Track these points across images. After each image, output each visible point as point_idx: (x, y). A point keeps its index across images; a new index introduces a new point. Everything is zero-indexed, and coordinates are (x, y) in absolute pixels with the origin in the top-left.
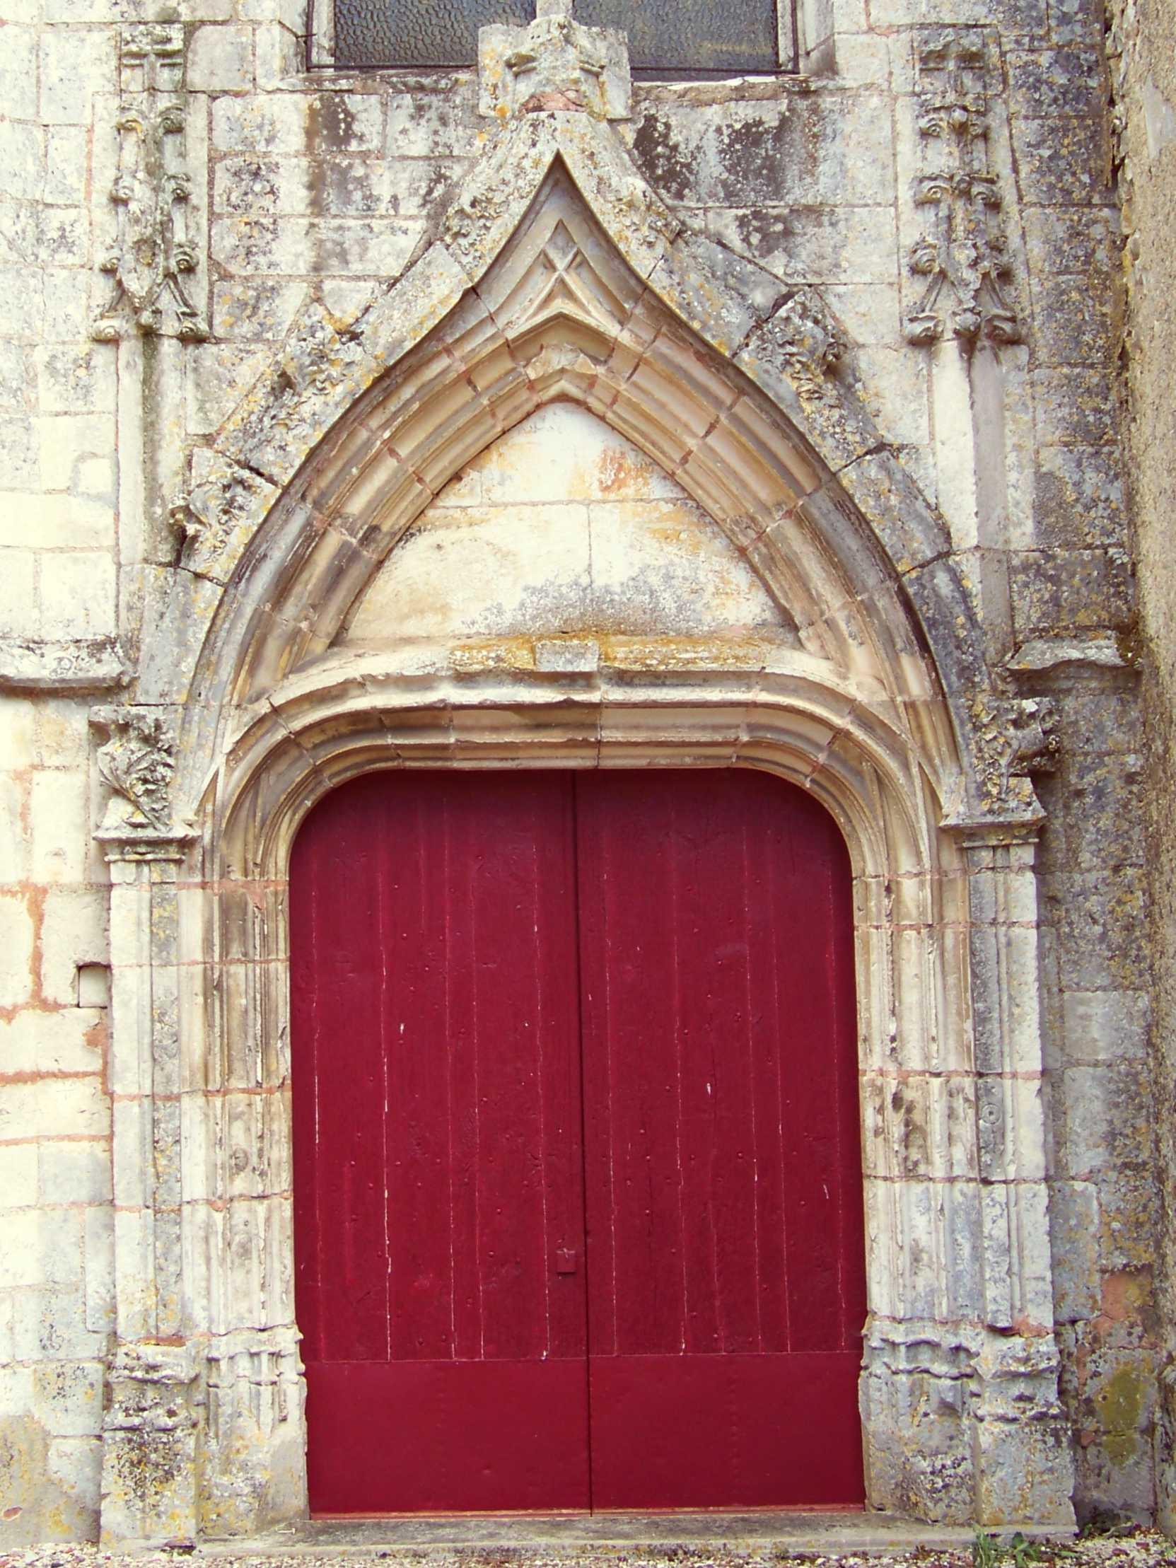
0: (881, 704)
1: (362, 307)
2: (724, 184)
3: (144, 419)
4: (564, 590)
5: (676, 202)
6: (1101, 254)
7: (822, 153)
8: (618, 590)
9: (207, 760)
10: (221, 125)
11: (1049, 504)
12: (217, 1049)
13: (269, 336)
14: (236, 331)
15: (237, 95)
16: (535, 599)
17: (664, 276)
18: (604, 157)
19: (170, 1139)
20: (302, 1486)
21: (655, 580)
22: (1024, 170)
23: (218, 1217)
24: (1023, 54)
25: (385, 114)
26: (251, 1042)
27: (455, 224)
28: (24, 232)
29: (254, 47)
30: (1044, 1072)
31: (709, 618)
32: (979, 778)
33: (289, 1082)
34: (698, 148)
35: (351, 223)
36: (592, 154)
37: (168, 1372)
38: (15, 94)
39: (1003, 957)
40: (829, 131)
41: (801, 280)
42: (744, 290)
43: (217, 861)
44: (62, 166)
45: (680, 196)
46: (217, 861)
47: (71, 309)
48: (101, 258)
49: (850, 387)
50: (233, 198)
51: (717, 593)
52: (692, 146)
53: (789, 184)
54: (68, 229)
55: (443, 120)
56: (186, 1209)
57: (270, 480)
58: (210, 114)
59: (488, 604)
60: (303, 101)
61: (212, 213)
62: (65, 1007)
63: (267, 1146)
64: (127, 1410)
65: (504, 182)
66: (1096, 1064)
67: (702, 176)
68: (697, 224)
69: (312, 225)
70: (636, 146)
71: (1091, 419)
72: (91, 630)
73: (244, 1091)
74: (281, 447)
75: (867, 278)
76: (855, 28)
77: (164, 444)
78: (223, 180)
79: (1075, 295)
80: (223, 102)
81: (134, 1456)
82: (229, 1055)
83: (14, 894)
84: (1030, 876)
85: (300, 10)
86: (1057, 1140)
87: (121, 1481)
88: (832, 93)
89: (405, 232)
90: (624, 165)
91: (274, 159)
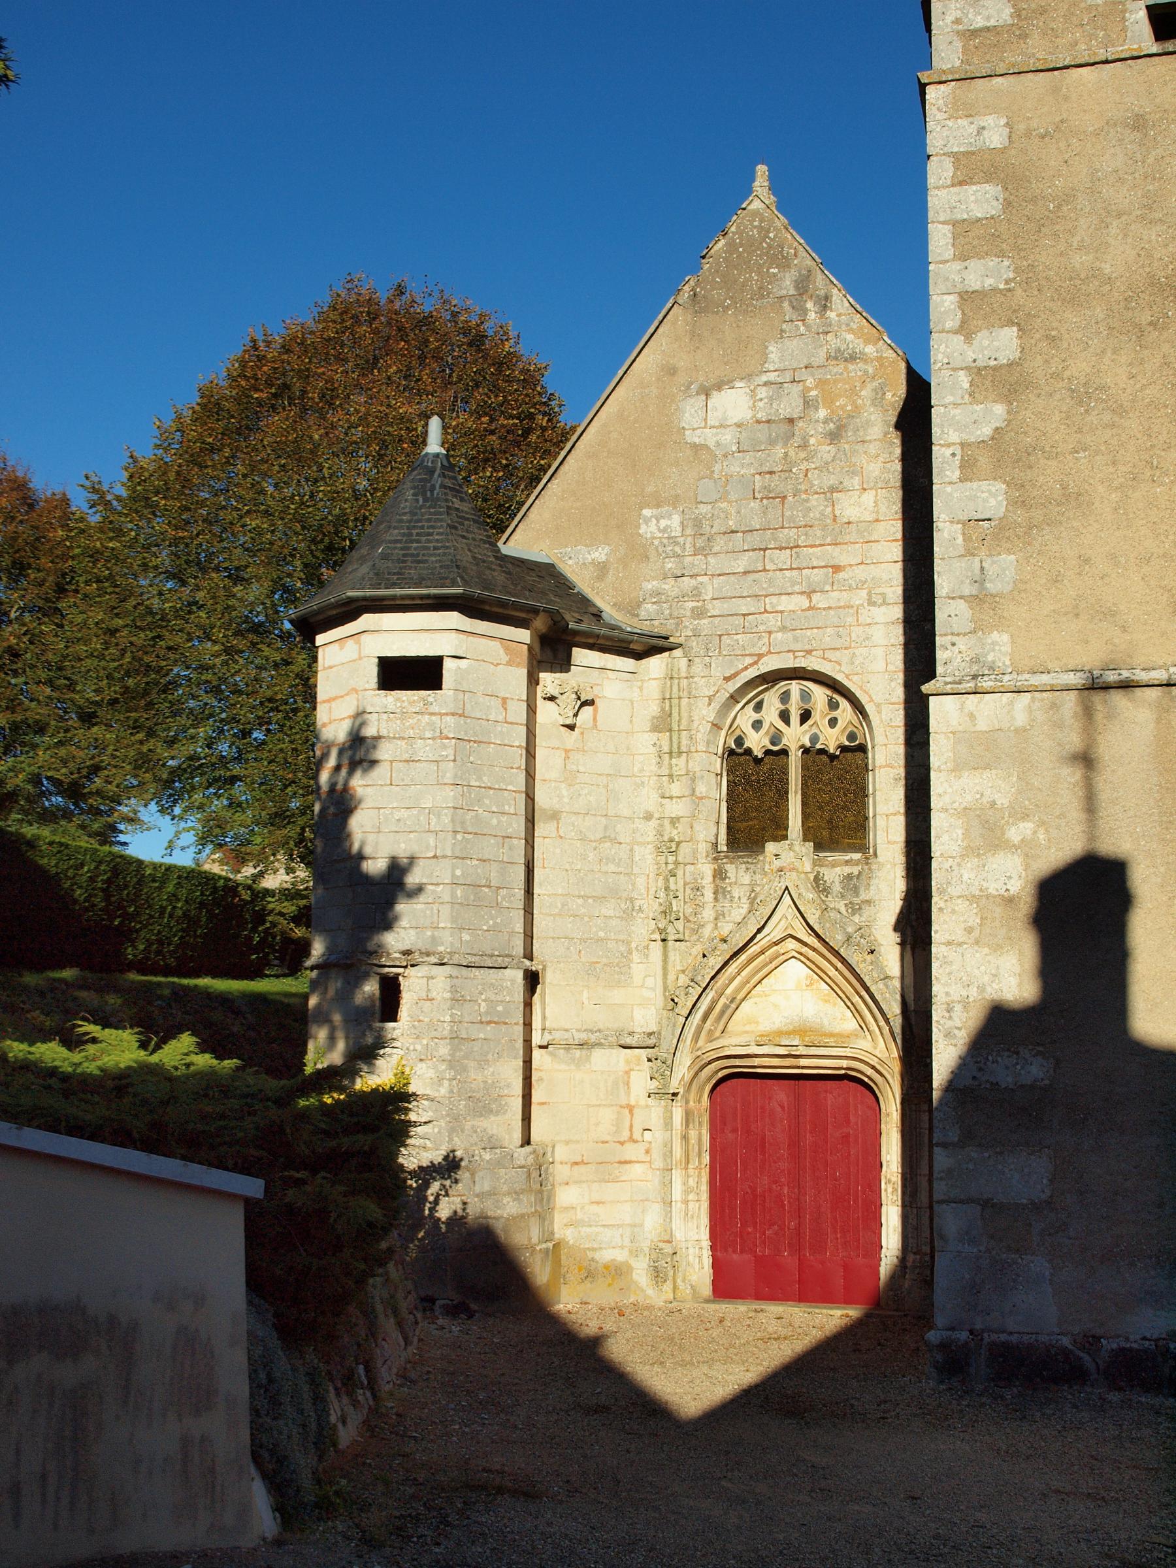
10: (687, 874)
18: (801, 886)
48: (651, 915)
60: (712, 866)
68: (832, 906)
78: (688, 891)
80: (688, 867)
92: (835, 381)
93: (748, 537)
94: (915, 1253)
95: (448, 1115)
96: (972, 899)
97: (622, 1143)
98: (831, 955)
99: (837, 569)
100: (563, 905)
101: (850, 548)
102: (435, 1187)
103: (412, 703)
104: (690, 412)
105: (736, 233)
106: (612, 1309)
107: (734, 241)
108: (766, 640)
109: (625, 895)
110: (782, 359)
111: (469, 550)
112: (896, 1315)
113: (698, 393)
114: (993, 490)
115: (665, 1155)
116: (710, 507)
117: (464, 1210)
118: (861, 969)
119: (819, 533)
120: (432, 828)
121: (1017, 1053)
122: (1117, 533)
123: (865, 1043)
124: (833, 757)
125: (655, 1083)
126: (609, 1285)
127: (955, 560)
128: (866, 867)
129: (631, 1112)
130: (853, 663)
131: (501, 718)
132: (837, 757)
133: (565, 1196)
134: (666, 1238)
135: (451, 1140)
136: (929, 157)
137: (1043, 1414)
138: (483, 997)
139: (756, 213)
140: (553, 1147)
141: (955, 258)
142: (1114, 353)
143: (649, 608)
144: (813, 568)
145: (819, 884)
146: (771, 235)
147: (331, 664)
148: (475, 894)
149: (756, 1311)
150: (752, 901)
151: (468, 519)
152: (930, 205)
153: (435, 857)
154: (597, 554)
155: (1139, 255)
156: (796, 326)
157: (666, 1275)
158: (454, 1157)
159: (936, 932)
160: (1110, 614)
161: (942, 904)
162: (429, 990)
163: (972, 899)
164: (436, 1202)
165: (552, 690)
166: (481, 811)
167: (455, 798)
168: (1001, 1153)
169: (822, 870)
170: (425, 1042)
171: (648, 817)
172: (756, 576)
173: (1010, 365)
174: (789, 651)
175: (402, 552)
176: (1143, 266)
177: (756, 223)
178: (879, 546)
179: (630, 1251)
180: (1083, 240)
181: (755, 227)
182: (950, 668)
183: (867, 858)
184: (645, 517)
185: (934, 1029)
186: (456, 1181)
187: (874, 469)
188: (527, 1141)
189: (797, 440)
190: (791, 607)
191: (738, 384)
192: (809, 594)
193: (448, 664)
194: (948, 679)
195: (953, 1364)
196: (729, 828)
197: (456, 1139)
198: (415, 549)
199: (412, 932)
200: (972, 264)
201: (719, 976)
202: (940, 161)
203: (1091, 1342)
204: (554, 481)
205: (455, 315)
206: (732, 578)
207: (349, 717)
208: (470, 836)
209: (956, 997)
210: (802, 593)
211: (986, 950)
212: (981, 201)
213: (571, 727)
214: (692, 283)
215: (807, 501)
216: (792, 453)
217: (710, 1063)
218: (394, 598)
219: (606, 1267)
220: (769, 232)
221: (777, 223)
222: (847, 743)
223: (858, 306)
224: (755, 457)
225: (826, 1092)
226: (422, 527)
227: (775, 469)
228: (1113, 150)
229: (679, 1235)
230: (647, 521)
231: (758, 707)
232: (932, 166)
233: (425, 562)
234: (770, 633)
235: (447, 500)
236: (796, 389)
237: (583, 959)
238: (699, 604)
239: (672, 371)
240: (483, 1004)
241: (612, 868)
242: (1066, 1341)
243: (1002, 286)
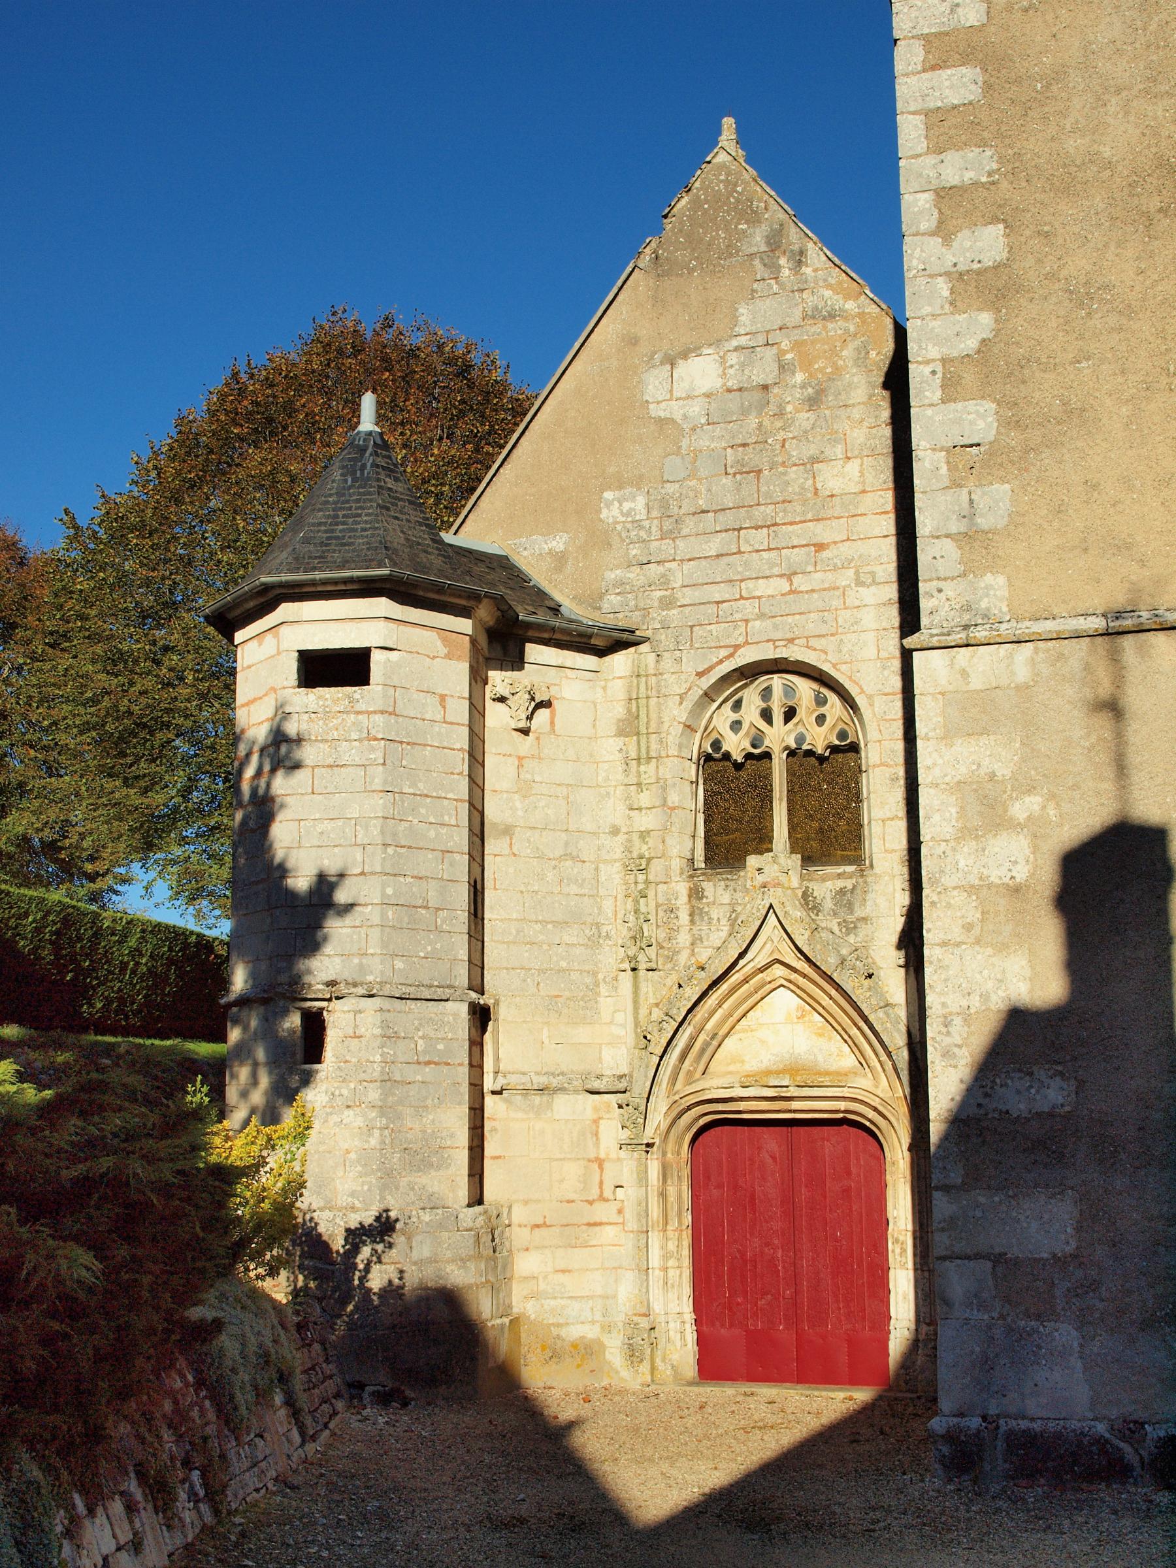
10: (660, 894)
18: (787, 904)
48: (620, 942)
55: (735, 890)
60: (687, 885)
68: (823, 925)
78: (661, 914)
80: (660, 886)
92: (812, 343)
93: (720, 516)
95: (379, 1170)
96: (971, 890)
97: (591, 1203)
98: (826, 984)
99: (820, 547)
100: (518, 932)
101: (834, 523)
102: (366, 1252)
103: (336, 701)
104: (654, 384)
105: (701, 189)
107: (698, 197)
108: (743, 629)
109: (589, 920)
110: (753, 322)
111: (402, 532)
112: (909, 1393)
113: (662, 363)
114: (982, 410)
115: (639, 1214)
116: (677, 485)
117: (401, 1279)
118: (858, 996)
119: (799, 509)
120: (359, 841)
121: (1031, 1074)
122: (1130, 452)
123: (865, 1082)
124: (822, 759)
126: (578, 1366)
127: (939, 493)
128: (861, 880)
129: (601, 1167)
130: (840, 651)
131: (439, 717)
132: (827, 758)
133: (525, 1264)
134: (644, 1310)
135: (383, 1198)
136: (896, 41)
137: (1073, 1523)
138: (420, 1033)
139: (723, 166)
140: (510, 1207)
141: (929, 151)
142: (1118, 246)
143: (612, 601)
144: (793, 547)
145: (808, 901)
146: (739, 189)
147: (250, 663)
148: (410, 913)
149: (745, 1394)
150: (733, 922)
151: (401, 500)
152: (898, 94)
153: (362, 873)
154: (554, 543)
155: (1143, 134)
156: (769, 285)
158: (388, 1217)
159: (929, 931)
160: (1125, 547)
161: (935, 898)
162: (356, 1026)
163: (971, 890)
164: (367, 1269)
165: (503, 690)
166: (416, 821)
167: (385, 806)
168: (1014, 1196)
169: (811, 885)
170: (352, 1086)
171: (615, 831)
172: (731, 558)
173: (997, 267)
174: (768, 641)
175: (325, 535)
176: (1149, 146)
177: (722, 178)
178: (866, 519)
179: (602, 1328)
180: (1077, 122)
181: (722, 181)
182: (936, 619)
183: (862, 870)
184: (606, 500)
185: (930, 1048)
186: (390, 1246)
187: (858, 435)
188: (477, 1199)
189: (772, 409)
190: (770, 592)
191: (706, 351)
192: (789, 577)
193: (376, 657)
194: (934, 631)
195: (963, 1457)
196: (707, 842)
197: (389, 1197)
198: (341, 531)
199: (337, 960)
200: (949, 156)
201: (697, 1009)
202: (909, 45)
203: (1132, 1429)
204: (507, 466)
205: (440, 347)
206: (703, 562)
207: (268, 720)
208: (403, 850)
209: (954, 1008)
210: (781, 576)
211: (989, 951)
212: (958, 85)
213: (525, 732)
214: (653, 245)
215: (785, 474)
216: (766, 423)
217: (689, 1108)
218: (313, 583)
219: (575, 1346)
220: (736, 185)
221: (746, 176)
222: (837, 742)
223: (836, 260)
224: (726, 429)
225: (823, 1139)
226: (350, 509)
227: (749, 441)
228: (1108, 19)
229: (657, 1307)
230: (609, 505)
231: (737, 706)
232: (900, 52)
233: (353, 544)
234: (747, 621)
235: (378, 480)
236: (770, 353)
237: (542, 993)
238: (668, 593)
239: (634, 341)
240: (420, 1042)
241: (574, 889)
242: (1101, 1428)
243: (984, 179)
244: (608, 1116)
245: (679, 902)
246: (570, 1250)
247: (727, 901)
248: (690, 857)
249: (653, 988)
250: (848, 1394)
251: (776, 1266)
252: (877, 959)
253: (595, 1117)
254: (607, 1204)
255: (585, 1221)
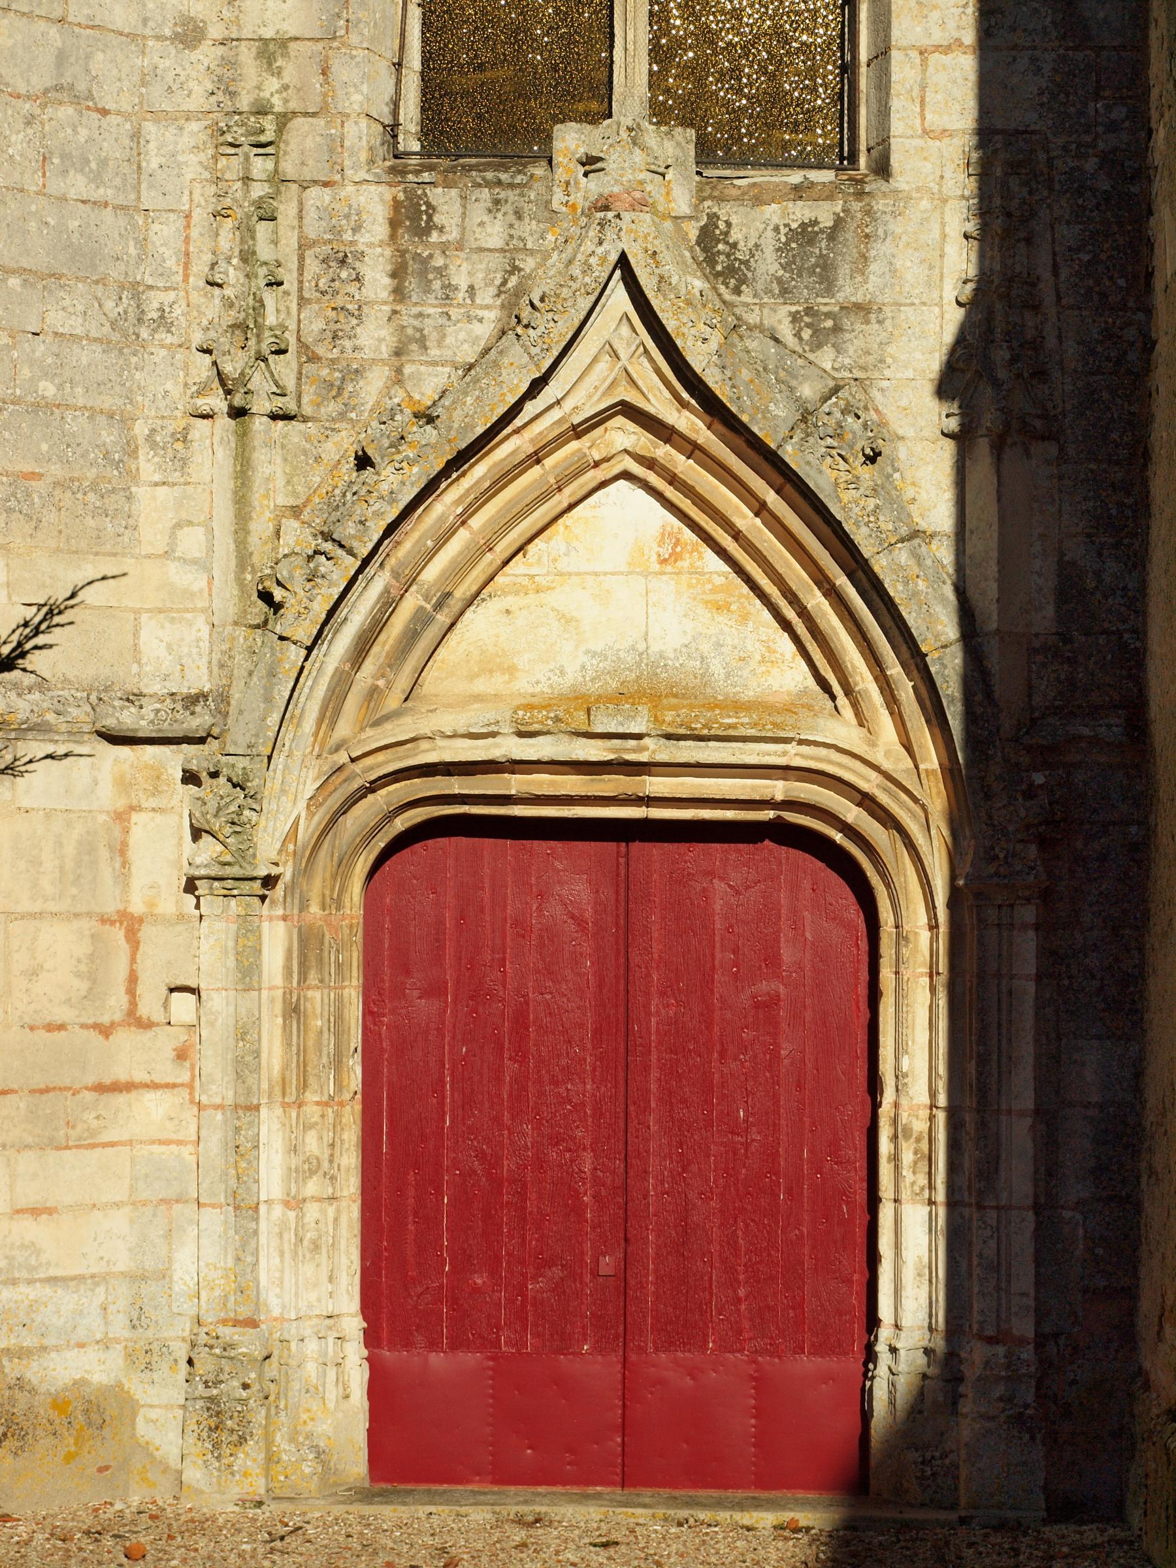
0: (907, 771)
1: (439, 390)
2: (780, 281)
3: (236, 493)
4: (622, 654)
5: (734, 298)
6: (1132, 356)
7: (873, 253)
8: (672, 656)
9: (290, 805)
10: (311, 215)
11: (1069, 588)
12: (294, 1065)
13: (353, 415)
14: (323, 410)
15: (326, 184)
16: (594, 662)
17: (716, 371)
18: (665, 256)
19: (249, 1145)
20: (364, 1455)
21: (705, 647)
22: (1064, 273)
23: (292, 1215)
24: (1069, 160)
25: (464, 207)
26: (325, 1060)
27: (526, 313)
28: (126, 312)
29: (342, 141)
30: (1037, 1111)
31: (755, 684)
32: (987, 843)
33: (359, 1096)
34: (757, 246)
35: (431, 311)
36: (655, 253)
37: (244, 1350)
38: (118, 181)
39: (1004, 1006)
40: (880, 232)
41: (847, 374)
42: (794, 383)
43: (297, 896)
44: (162, 250)
45: (737, 291)
46: (297, 896)
47: (169, 386)
48: (198, 338)
49: (889, 476)
50: (321, 285)
51: (763, 661)
52: (751, 244)
53: (840, 282)
54: (167, 310)
55: (519, 215)
56: (263, 1209)
57: (351, 552)
58: (301, 203)
59: (552, 666)
60: (388, 193)
61: (301, 298)
62: (158, 1025)
63: (337, 1154)
64: (206, 1382)
65: (572, 278)
66: (1088, 1105)
67: (759, 272)
68: (752, 318)
69: (395, 312)
70: (698, 243)
71: (1114, 512)
72: (185, 684)
73: (317, 1103)
74: (361, 522)
75: (910, 374)
76: (910, 132)
77: (254, 515)
78: (313, 266)
79: (1105, 395)
80: (314, 191)
81: (213, 1422)
82: (305, 1071)
83: (113, 923)
84: (1031, 934)
85: (387, 99)
86: (1048, 1170)
87: (200, 1444)
88: (884, 195)
89: (481, 320)
90: (684, 263)
91: (361, 247)
94: (991, 1341)
97: (105, 1031)
98: (752, 473)
106: (94, 1535)
109: (115, 272)
115: (239, 1061)
118: (848, 507)
125: (209, 848)
126: (69, 1457)
128: (856, 206)
134: (244, 1312)
149: (520, 1521)
157: (244, 1422)
169: (723, 211)
171: (189, 34)
179: (130, 1356)
201: (406, 526)
217: (373, 787)
219: (60, 1404)
225: (710, 874)
229: (274, 1302)
244: (152, 803)
245: (363, 239)
246: (52, 1156)
247: (496, 242)
248: (388, 120)
249: (288, 466)
250: (786, 1516)
251: (577, 1196)
252: (891, 414)
253: (121, 804)
254: (146, 1036)
255: (91, 1080)
